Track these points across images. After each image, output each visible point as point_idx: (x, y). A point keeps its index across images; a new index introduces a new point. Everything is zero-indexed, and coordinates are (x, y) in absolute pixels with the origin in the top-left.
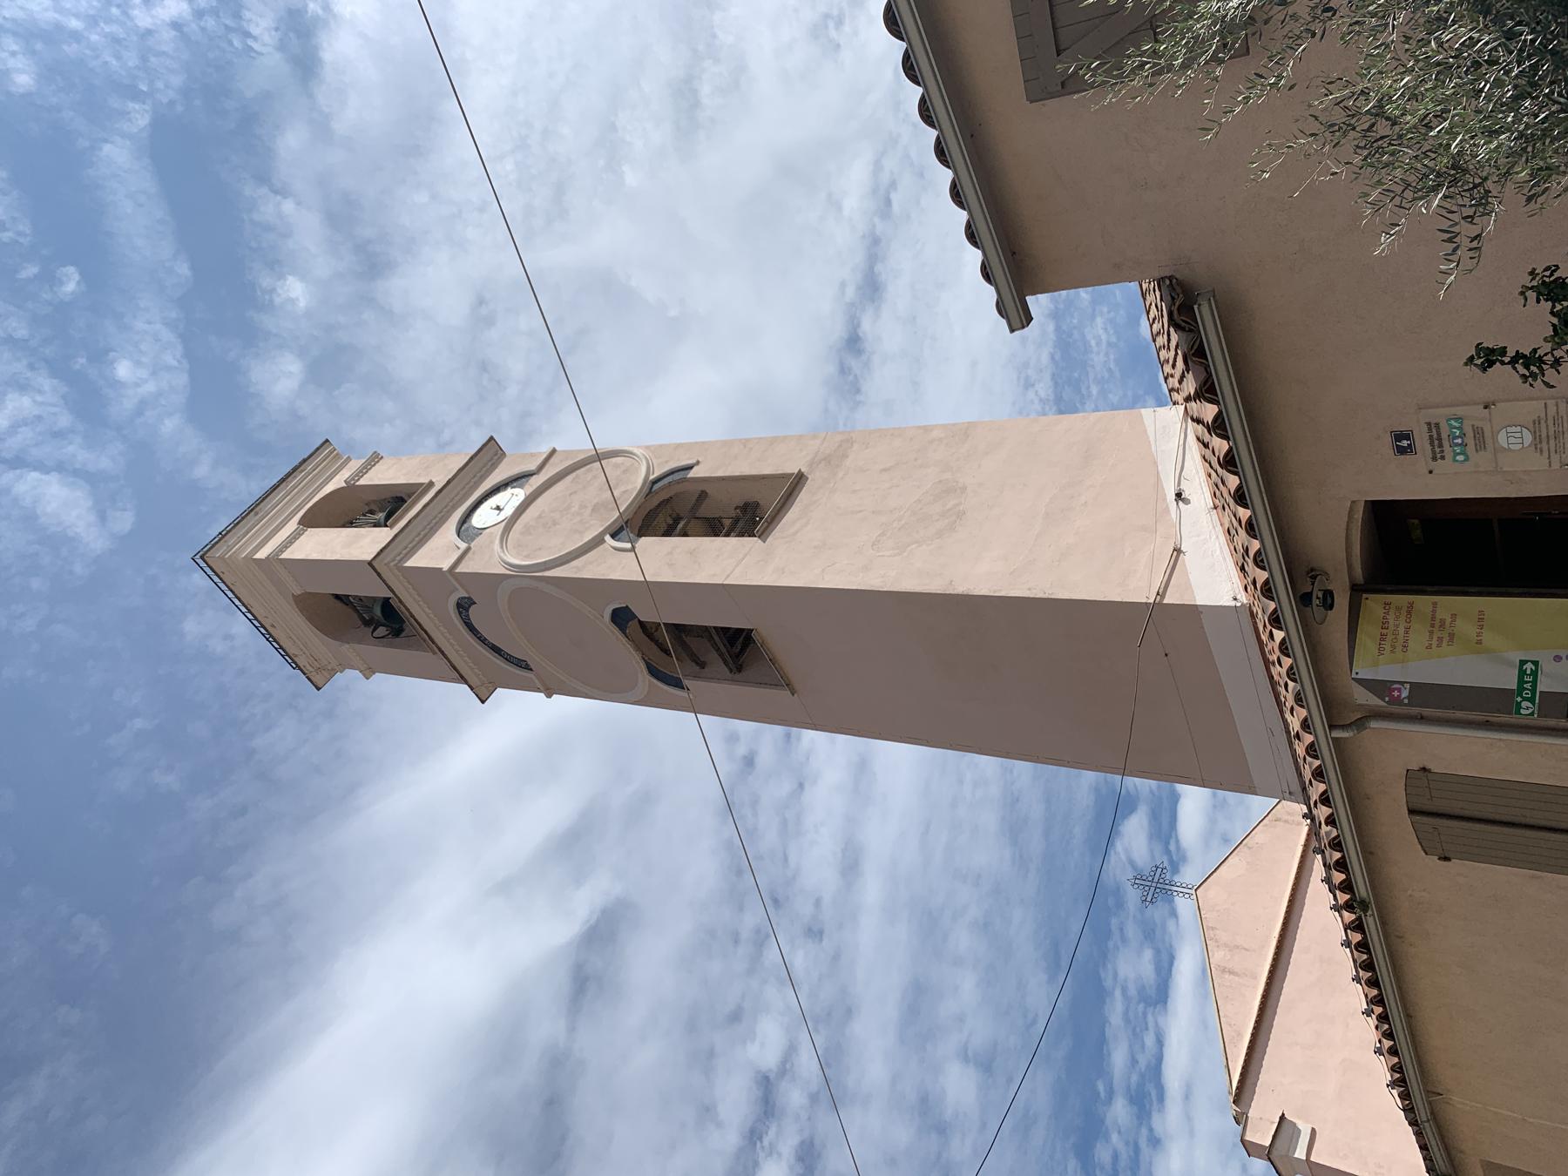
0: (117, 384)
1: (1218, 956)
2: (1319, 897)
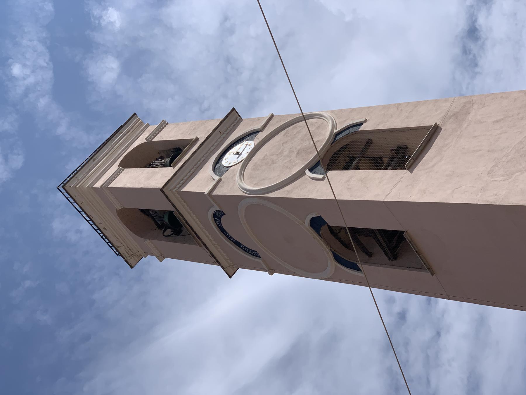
0: (13, 79)
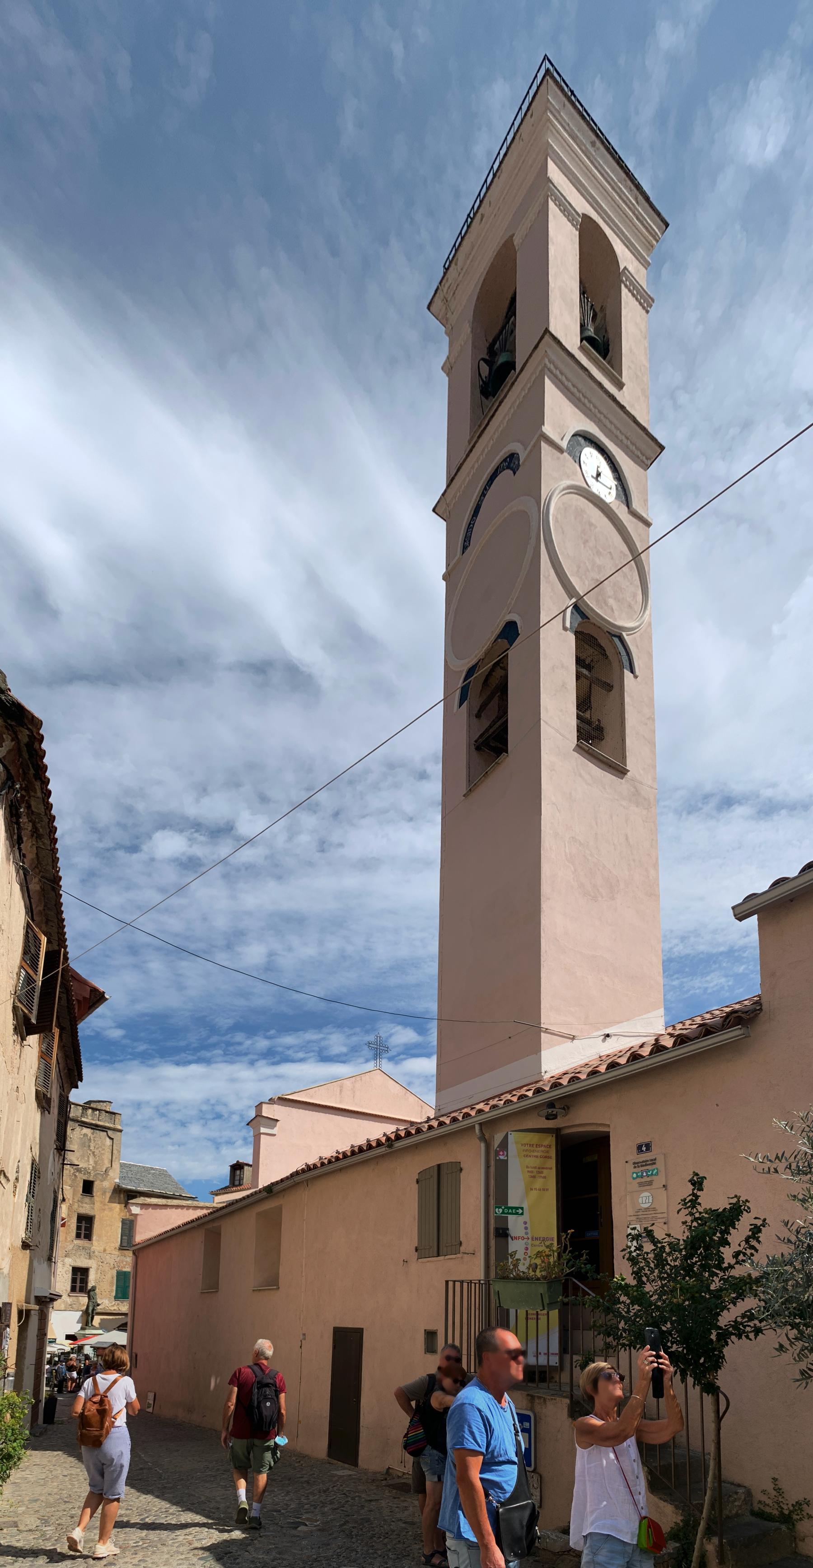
1: (348, 1083)
2: (390, 1129)
